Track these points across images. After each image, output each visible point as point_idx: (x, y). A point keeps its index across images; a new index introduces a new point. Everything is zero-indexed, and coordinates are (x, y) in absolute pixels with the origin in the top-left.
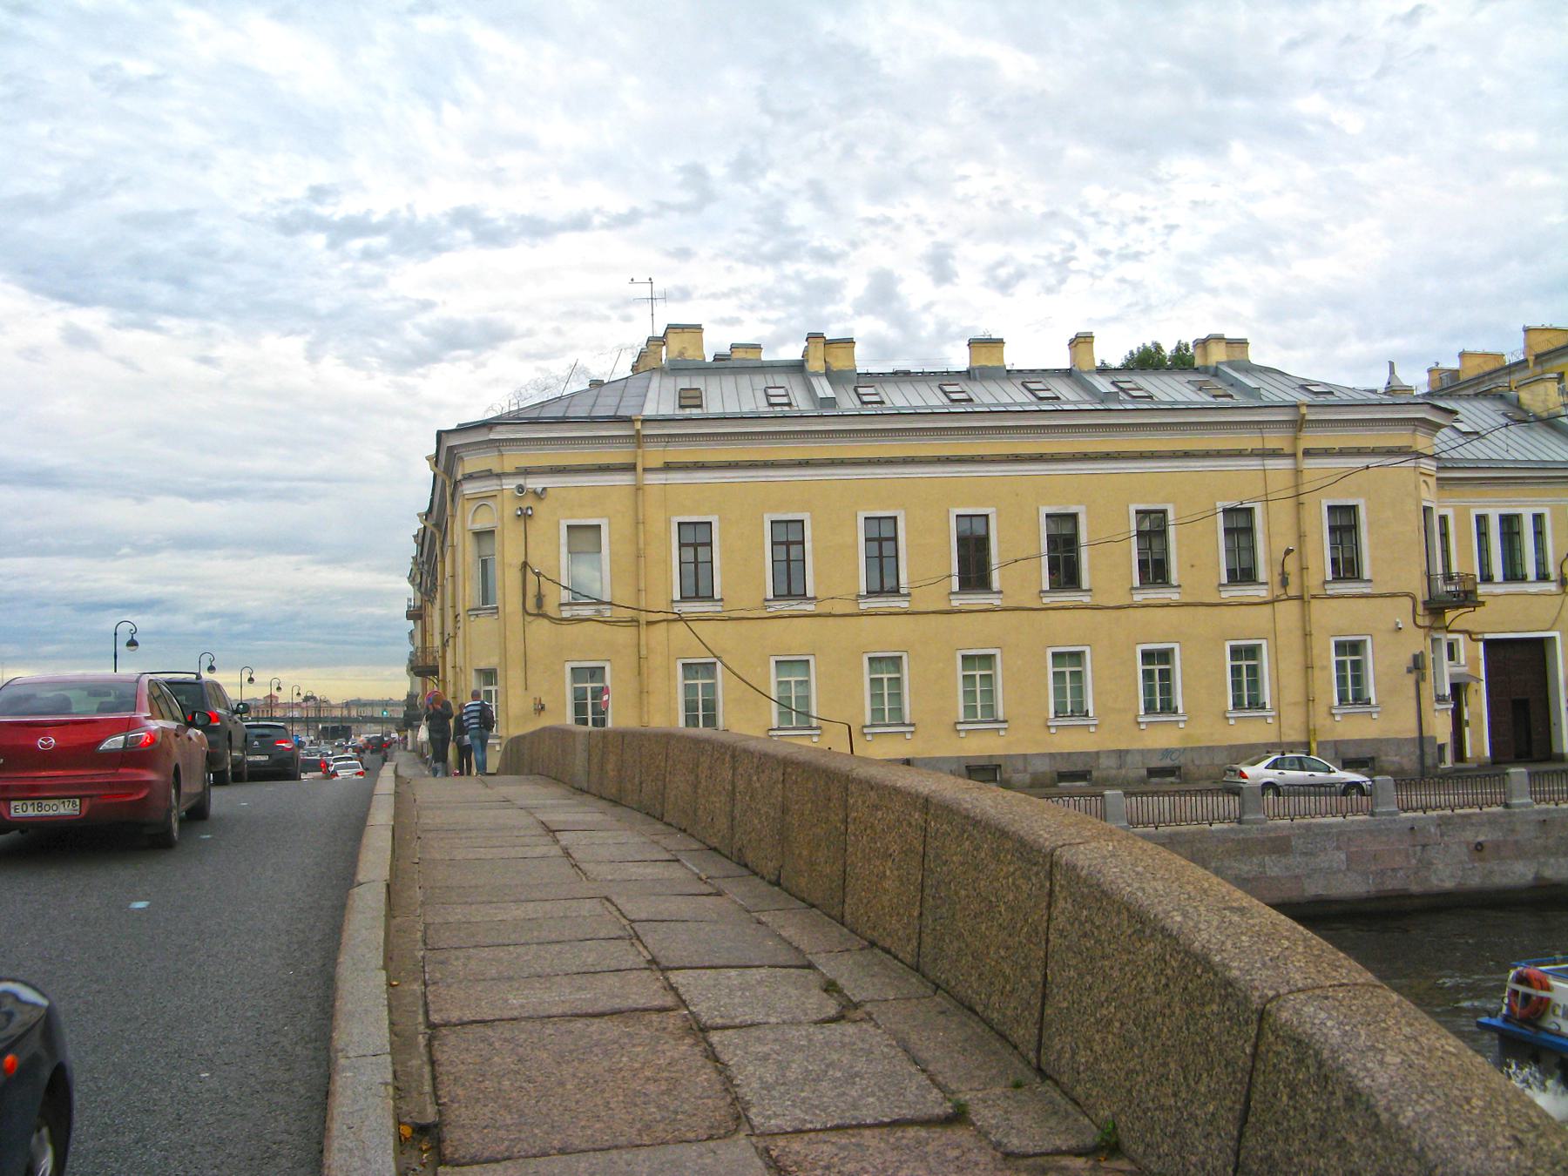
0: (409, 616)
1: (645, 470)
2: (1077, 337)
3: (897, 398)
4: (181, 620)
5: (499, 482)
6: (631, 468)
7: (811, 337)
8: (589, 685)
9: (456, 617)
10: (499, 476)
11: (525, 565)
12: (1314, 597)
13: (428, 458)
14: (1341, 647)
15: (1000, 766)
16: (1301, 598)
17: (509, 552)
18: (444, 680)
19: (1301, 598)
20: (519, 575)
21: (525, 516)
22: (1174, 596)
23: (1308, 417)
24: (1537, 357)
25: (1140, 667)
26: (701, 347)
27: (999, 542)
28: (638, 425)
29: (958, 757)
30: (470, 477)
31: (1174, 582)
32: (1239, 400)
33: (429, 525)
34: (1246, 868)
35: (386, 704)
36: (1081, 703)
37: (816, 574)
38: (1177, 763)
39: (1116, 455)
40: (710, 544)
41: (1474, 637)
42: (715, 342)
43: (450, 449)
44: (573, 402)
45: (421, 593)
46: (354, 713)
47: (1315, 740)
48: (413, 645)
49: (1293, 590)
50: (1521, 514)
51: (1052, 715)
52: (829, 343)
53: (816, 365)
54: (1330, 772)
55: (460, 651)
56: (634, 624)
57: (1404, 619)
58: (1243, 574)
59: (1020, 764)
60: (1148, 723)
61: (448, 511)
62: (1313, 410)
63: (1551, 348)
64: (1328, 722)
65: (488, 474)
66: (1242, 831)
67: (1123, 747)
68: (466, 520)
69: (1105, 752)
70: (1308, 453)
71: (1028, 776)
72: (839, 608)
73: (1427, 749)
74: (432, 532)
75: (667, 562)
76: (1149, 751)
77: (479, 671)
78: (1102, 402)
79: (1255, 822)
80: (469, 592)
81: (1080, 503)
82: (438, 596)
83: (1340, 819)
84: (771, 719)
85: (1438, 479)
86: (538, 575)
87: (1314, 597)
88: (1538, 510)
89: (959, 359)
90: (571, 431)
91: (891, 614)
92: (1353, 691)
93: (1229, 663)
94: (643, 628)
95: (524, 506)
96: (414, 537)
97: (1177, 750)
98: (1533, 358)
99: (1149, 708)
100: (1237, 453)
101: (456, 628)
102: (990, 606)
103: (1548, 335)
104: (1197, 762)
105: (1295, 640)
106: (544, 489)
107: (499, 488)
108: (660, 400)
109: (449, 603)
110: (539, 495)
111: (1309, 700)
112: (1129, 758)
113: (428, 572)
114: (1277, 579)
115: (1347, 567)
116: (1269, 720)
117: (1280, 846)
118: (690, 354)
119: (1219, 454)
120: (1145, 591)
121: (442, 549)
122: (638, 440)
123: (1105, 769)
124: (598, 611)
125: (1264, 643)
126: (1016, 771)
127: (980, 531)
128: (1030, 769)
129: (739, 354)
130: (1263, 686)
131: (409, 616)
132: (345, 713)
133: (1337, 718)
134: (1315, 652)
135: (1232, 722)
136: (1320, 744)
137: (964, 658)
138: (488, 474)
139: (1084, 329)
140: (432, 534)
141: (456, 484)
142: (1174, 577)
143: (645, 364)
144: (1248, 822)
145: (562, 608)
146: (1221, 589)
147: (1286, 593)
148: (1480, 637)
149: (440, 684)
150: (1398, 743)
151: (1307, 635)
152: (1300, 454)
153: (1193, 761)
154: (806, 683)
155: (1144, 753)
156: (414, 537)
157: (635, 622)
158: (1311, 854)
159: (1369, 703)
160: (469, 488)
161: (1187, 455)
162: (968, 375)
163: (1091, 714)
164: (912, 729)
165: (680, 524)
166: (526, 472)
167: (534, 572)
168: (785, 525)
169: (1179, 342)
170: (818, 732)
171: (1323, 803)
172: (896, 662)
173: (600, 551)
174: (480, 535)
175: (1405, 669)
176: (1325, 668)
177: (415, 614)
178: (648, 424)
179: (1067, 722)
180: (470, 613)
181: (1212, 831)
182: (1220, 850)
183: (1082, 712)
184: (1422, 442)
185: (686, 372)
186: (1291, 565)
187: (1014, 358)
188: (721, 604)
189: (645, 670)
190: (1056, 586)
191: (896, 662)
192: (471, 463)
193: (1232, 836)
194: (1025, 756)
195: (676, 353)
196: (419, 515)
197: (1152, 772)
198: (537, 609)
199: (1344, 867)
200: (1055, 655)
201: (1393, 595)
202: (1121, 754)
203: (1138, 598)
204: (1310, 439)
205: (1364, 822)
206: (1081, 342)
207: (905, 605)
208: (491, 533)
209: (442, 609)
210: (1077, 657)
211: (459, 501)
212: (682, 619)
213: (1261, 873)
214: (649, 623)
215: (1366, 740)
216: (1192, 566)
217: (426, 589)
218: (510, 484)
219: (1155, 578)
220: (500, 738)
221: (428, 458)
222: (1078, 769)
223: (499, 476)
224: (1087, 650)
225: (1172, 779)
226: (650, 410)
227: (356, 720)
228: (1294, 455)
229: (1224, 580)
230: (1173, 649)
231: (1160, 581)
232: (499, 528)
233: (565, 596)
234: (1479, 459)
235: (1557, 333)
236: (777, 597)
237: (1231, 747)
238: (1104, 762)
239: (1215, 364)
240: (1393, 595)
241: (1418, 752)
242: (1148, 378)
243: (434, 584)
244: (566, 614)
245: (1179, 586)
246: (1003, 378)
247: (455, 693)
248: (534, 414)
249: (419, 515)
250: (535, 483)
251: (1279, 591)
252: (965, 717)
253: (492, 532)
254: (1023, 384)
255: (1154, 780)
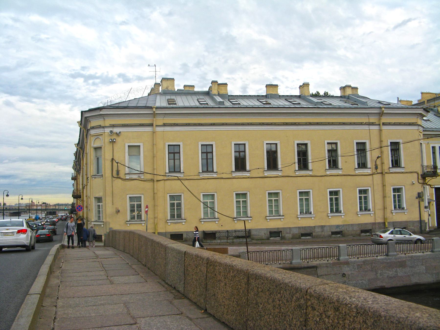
0: (72, 179)
1: (156, 126)
2: (303, 84)
3: (244, 103)
4: (16, 181)
5: (103, 130)
6: (151, 125)
7: (213, 82)
8: (136, 203)
9: (87, 178)
10: (104, 127)
11: (113, 159)
12: (386, 173)
13: (78, 122)
14: (394, 190)
15: (281, 231)
16: (382, 173)
17: (107, 154)
18: (83, 200)
19: (382, 173)
20: (110, 163)
21: (113, 142)
22: (340, 172)
23: (384, 112)
24: (428, 101)
25: (329, 197)
26: (174, 86)
27: (281, 153)
28: (154, 110)
29: (267, 228)
30: (93, 128)
31: (340, 168)
32: (360, 106)
33: (78, 148)
34: (391, 273)
35: (66, 205)
36: (308, 209)
37: (217, 164)
38: (341, 230)
39: (320, 123)
40: (179, 153)
41: (432, 186)
42: (179, 86)
43: (86, 118)
44: (130, 103)
45: (76, 171)
46: (57, 208)
47: (387, 222)
48: (74, 188)
49: (379, 171)
50: (435, 146)
51: (299, 213)
52: (219, 85)
53: (215, 91)
54: (410, 235)
55: (88, 192)
56: (152, 181)
57: (415, 181)
58: (362, 165)
59: (288, 231)
60: (331, 216)
61: (85, 142)
62: (386, 109)
63: (431, 98)
64: (391, 215)
65: (100, 127)
66: (389, 259)
67: (323, 224)
68: (92, 143)
69: (317, 226)
70: (384, 124)
71: (291, 235)
72: (224, 176)
73: (422, 224)
74: (79, 150)
75: (164, 158)
76: (332, 226)
77: (96, 198)
78: (315, 105)
79: (393, 255)
80: (92, 170)
81: (308, 140)
82: (81, 172)
83: (421, 254)
84: (201, 216)
85: (423, 134)
86: (117, 163)
87: (386, 173)
88: (433, 145)
89: (263, 92)
90: (129, 111)
91: (243, 178)
92: (399, 206)
93: (358, 195)
94: (155, 182)
95: (112, 138)
96: (74, 154)
97: (341, 225)
98: (426, 101)
99: (332, 211)
100: (360, 123)
101: (87, 182)
102: (278, 176)
103: (428, 95)
104: (348, 230)
105: (380, 188)
106: (120, 132)
107: (103, 132)
108: (161, 102)
109: (85, 174)
110: (118, 134)
111: (385, 208)
112: (325, 228)
113: (78, 164)
114: (374, 167)
115: (396, 163)
116: (372, 215)
117: (402, 264)
118: (170, 88)
119: (355, 124)
120: (330, 171)
121: (83, 156)
122: (154, 115)
123: (317, 232)
124: (139, 176)
125: (370, 188)
126: (287, 233)
127: (274, 149)
128: (291, 233)
129: (187, 89)
130: (369, 203)
131: (72, 179)
132: (54, 207)
133: (394, 214)
134: (387, 191)
135: (359, 216)
136: (388, 223)
137: (269, 193)
138: (100, 127)
139: (306, 81)
140: (80, 151)
141: (88, 130)
142: (340, 166)
143: (153, 92)
144: (391, 256)
145: (126, 175)
146: (356, 170)
147: (377, 171)
148: (433, 186)
149: (82, 201)
150: (413, 222)
151: (384, 186)
152: (381, 124)
153: (346, 229)
154: (213, 203)
155: (330, 226)
156: (74, 154)
157: (153, 180)
158: (413, 267)
159: (404, 209)
160: (92, 132)
161: (344, 124)
162: (266, 96)
163: (312, 213)
164: (251, 219)
165: (169, 145)
166: (113, 126)
167: (116, 162)
168: (206, 146)
169: (325, 92)
170: (218, 220)
171: (412, 246)
172: (245, 195)
173: (140, 155)
174: (96, 149)
175: (415, 198)
176: (389, 197)
177: (74, 178)
178: (158, 109)
179: (305, 216)
180: (92, 177)
181: (378, 259)
182: (381, 267)
183: (309, 212)
184: (420, 122)
185: (169, 94)
186: (379, 162)
187: (281, 92)
188: (183, 174)
189: (156, 198)
190: (300, 169)
191: (245, 195)
192: (94, 123)
193: (385, 261)
194: (290, 228)
195: (165, 88)
196: (75, 144)
197: (333, 233)
198: (117, 175)
199: (425, 272)
200: (300, 192)
201: (411, 172)
202: (322, 227)
203: (328, 173)
204: (385, 119)
205: (430, 254)
206: (305, 86)
207: (249, 175)
208: (100, 148)
209: (83, 176)
210: (307, 193)
211: (89, 137)
212: (179, 179)
213: (396, 275)
214: (157, 181)
215: (403, 221)
216: (346, 162)
217: (77, 170)
218: (108, 130)
219: (333, 166)
220: (104, 222)
221: (78, 122)
222: (308, 232)
223: (104, 127)
224: (311, 191)
225: (339, 235)
226: (158, 104)
227: (58, 210)
228: (379, 125)
229: (357, 167)
230: (339, 191)
231: (335, 167)
232: (104, 145)
233: (127, 170)
234: (428, 128)
235: (432, 94)
236: (203, 172)
237: (359, 224)
238: (317, 230)
239: (348, 95)
240: (411, 172)
241: (420, 225)
242: (330, 99)
243: (80, 168)
244: (128, 177)
245: (342, 169)
246: (278, 98)
247: (87, 205)
248: (117, 105)
249: (75, 144)
250: (116, 130)
251: (374, 171)
252: (269, 214)
253: (101, 148)
254: (285, 100)
255: (333, 236)
